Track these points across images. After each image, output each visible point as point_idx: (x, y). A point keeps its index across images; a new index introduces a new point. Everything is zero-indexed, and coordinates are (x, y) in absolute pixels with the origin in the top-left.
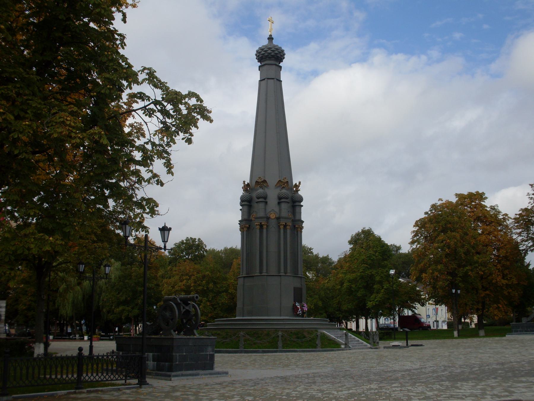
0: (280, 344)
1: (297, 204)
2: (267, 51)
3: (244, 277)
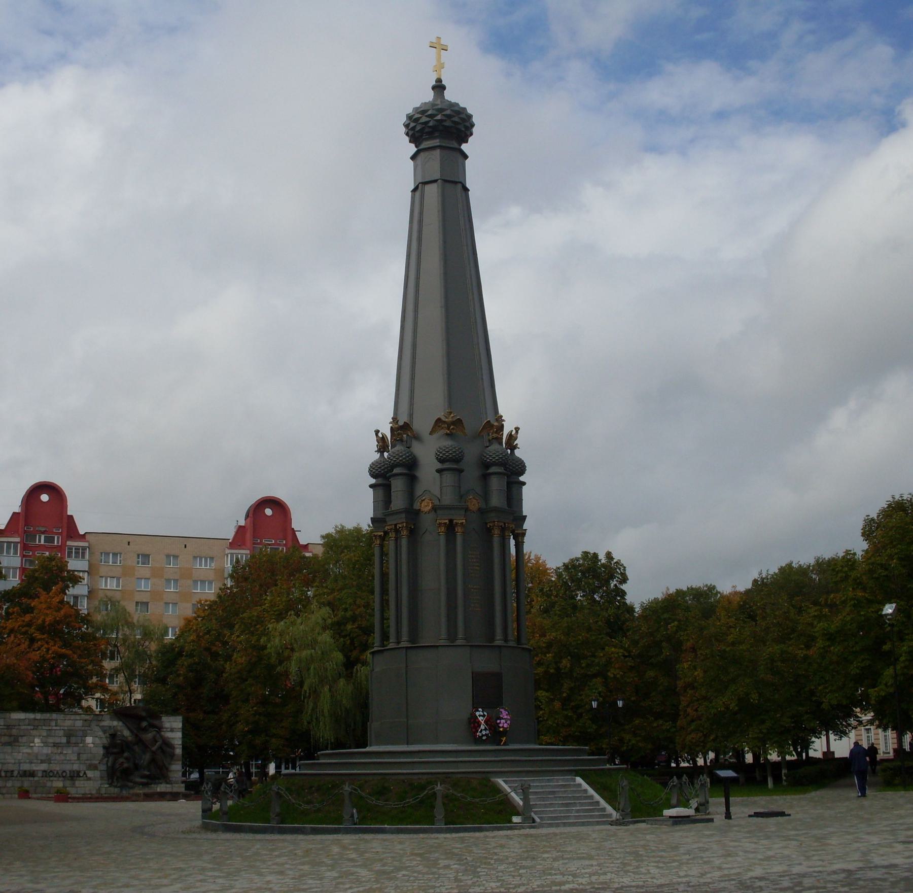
0: (439, 812)
1: (380, 481)
2: (418, 119)
3: (407, 648)
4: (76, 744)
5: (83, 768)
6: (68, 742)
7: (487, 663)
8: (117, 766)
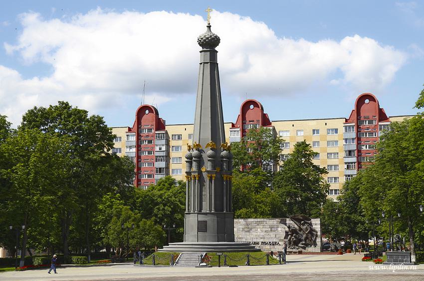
0: (22, 263)
4: (274, 231)
5: (277, 241)
6: (271, 230)
7: (202, 218)
8: (292, 240)
